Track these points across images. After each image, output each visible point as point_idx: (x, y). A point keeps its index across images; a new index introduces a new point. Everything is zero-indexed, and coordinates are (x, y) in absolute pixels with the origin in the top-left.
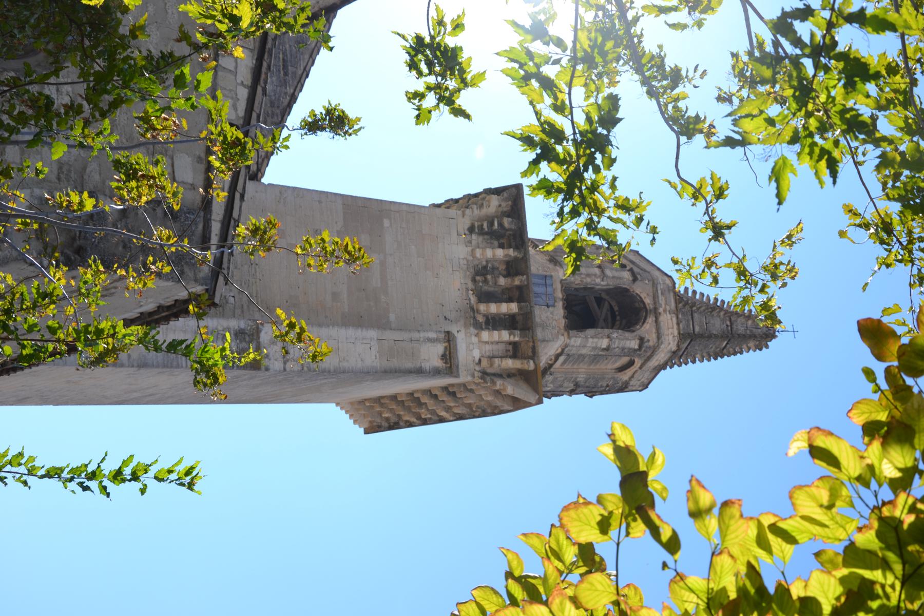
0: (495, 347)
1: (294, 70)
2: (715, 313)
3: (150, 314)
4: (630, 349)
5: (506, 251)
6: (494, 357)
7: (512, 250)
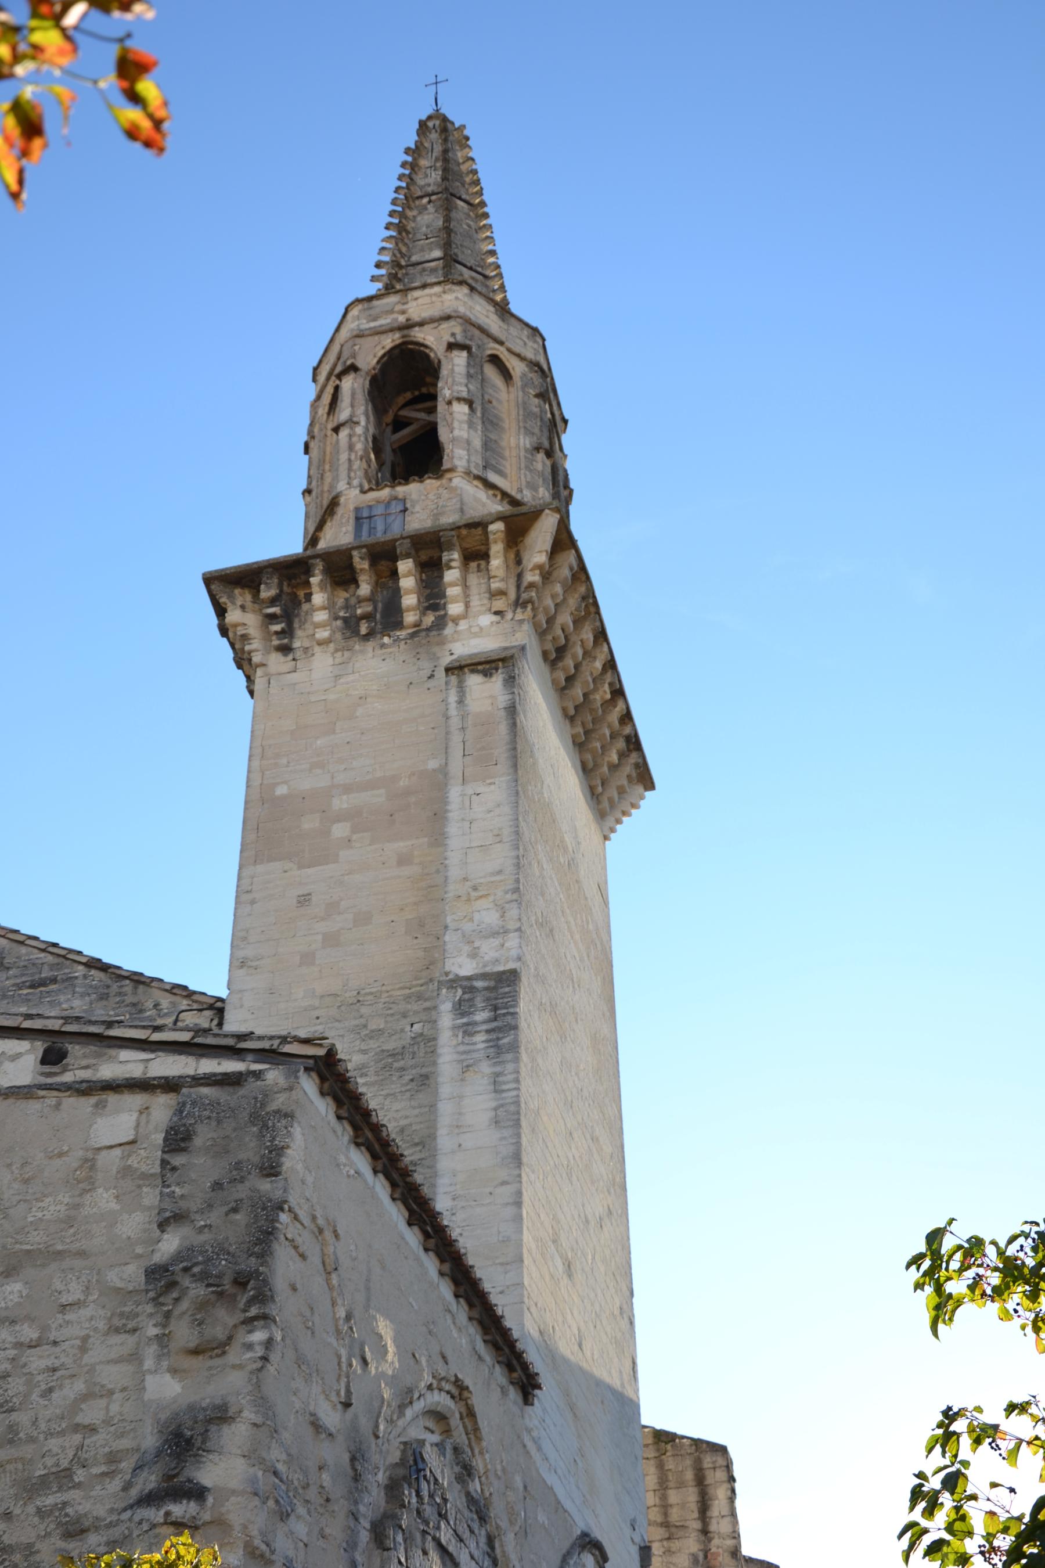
0: (474, 591)
1: (46, 967)
2: (410, 226)
3: (375, 1157)
4: (469, 365)
5: (315, 589)
7: (311, 579)
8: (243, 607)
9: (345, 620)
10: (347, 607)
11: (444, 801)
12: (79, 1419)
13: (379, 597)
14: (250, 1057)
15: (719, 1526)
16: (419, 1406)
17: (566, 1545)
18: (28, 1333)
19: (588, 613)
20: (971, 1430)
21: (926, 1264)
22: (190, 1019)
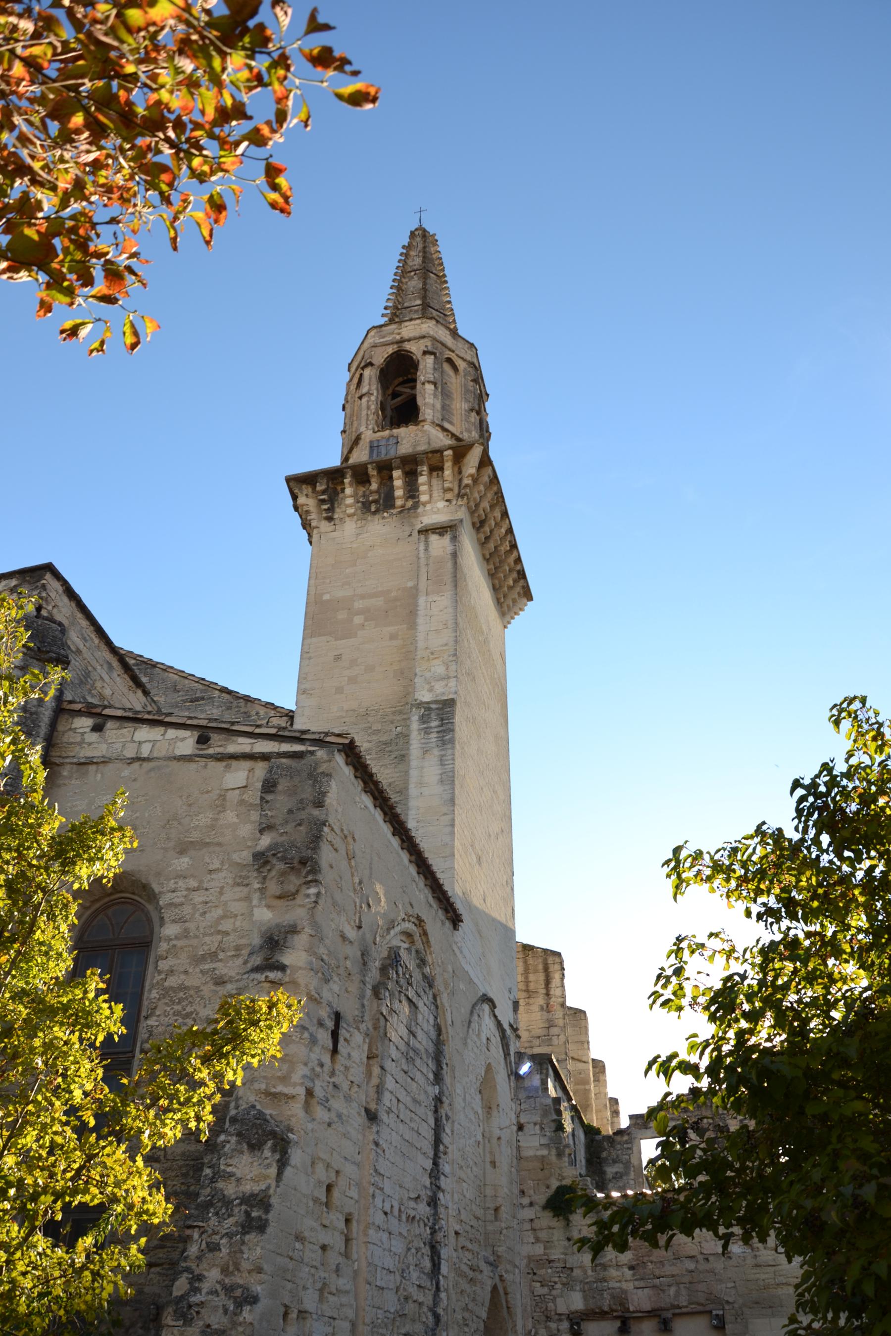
0: (435, 488)
2: (404, 287)
3: (375, 798)
5: (347, 485)
6: (443, 488)
8: (307, 495)
9: (363, 503)
10: (364, 496)
11: (416, 605)
12: (220, 928)
13: (382, 491)
14: (308, 743)
15: (555, 992)
16: (398, 929)
17: (475, 1000)
18: (193, 884)
19: (498, 502)
20: (690, 946)
21: (673, 864)
22: (275, 721)
